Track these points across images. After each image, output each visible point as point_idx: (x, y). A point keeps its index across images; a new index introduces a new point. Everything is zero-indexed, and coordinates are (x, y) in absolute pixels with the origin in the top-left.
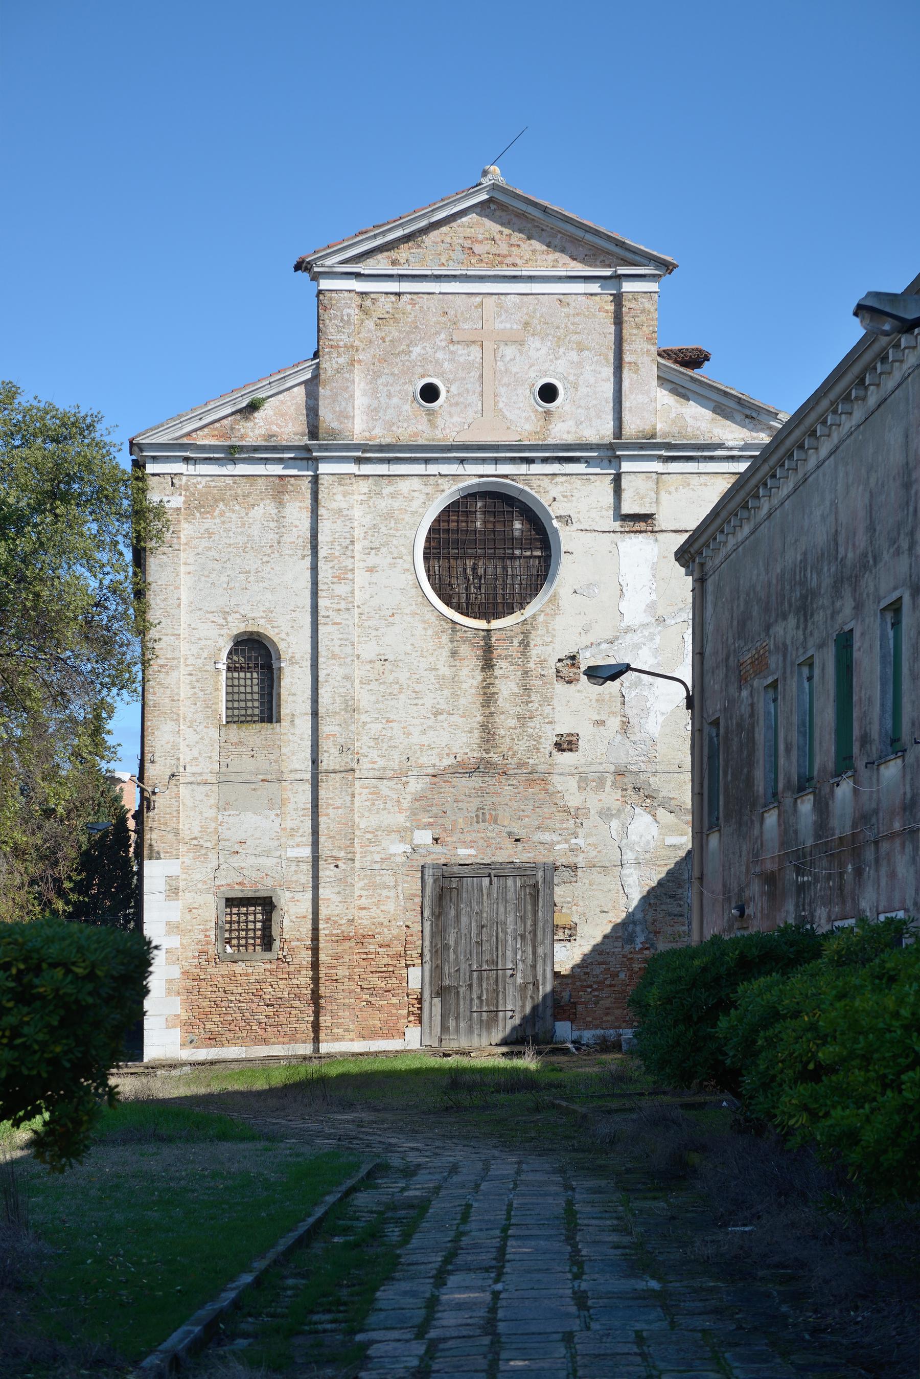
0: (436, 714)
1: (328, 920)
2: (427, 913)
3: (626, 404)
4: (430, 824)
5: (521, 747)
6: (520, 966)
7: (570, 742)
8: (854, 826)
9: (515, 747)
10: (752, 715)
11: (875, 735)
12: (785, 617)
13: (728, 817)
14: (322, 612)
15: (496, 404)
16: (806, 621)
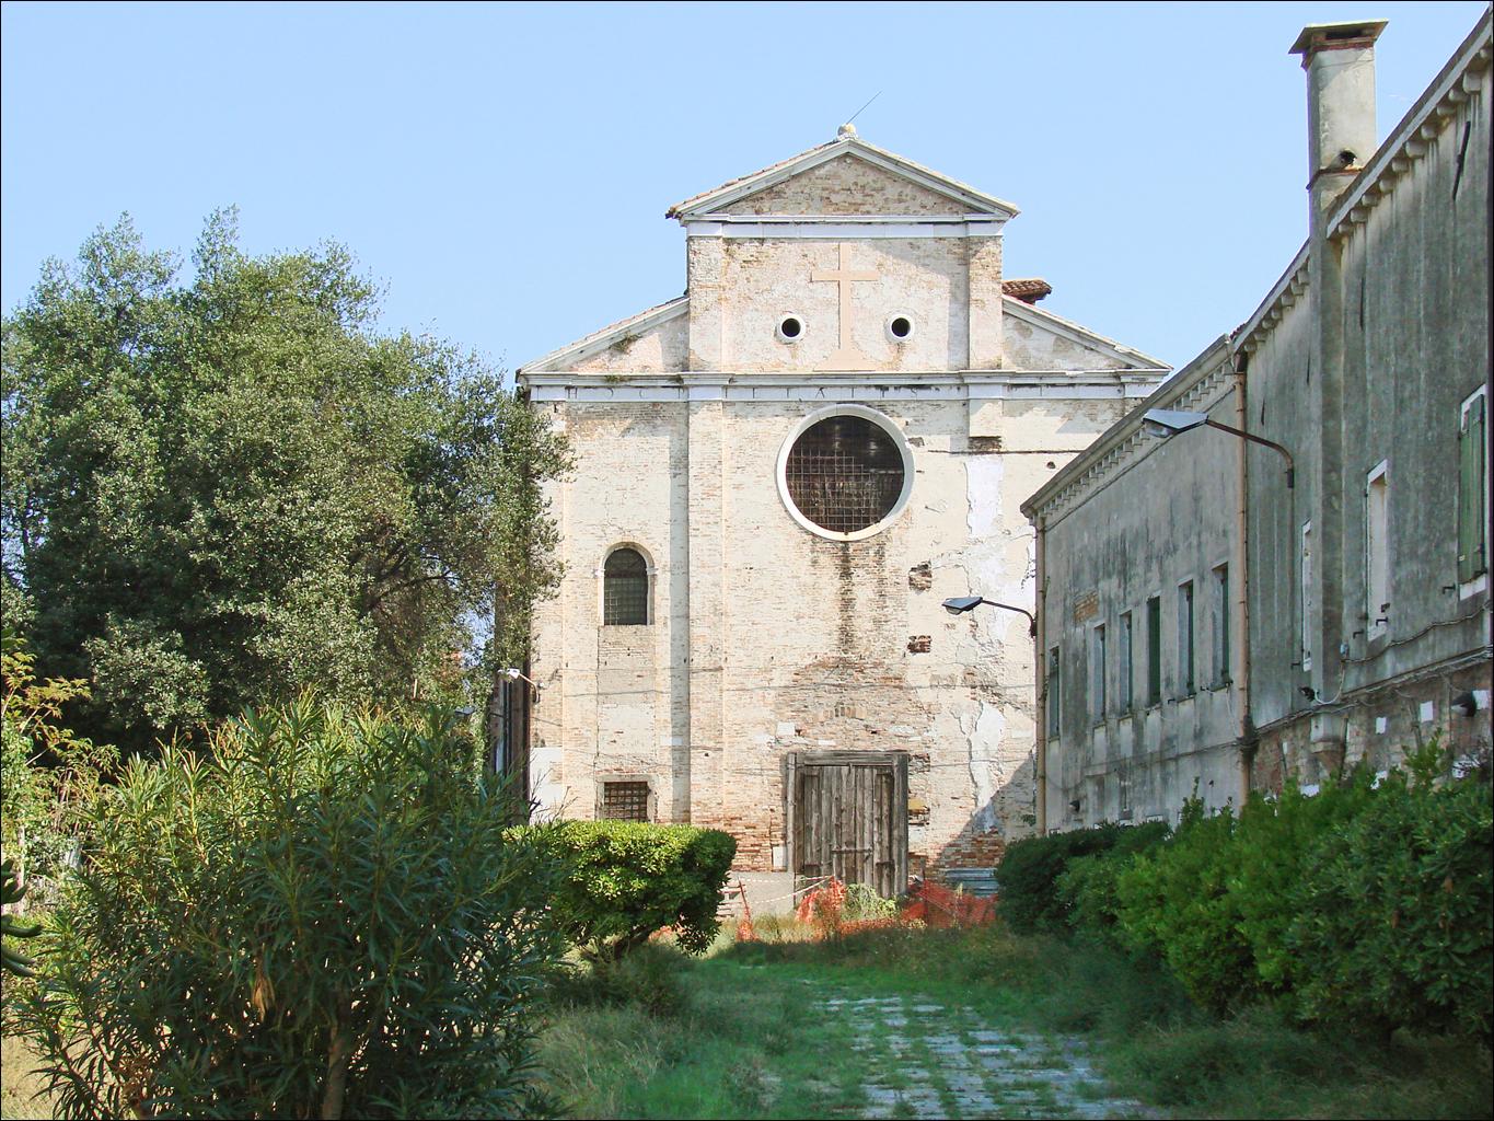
0: (798, 618)
1: (698, 803)
2: (790, 798)
3: (973, 338)
4: (793, 717)
5: (878, 647)
6: (877, 847)
7: (923, 644)
8: (1162, 743)
9: (872, 648)
10: (1085, 649)
11: (1175, 679)
12: (1109, 576)
13: (1066, 729)
14: (693, 525)
15: (852, 337)
16: (1126, 582)
